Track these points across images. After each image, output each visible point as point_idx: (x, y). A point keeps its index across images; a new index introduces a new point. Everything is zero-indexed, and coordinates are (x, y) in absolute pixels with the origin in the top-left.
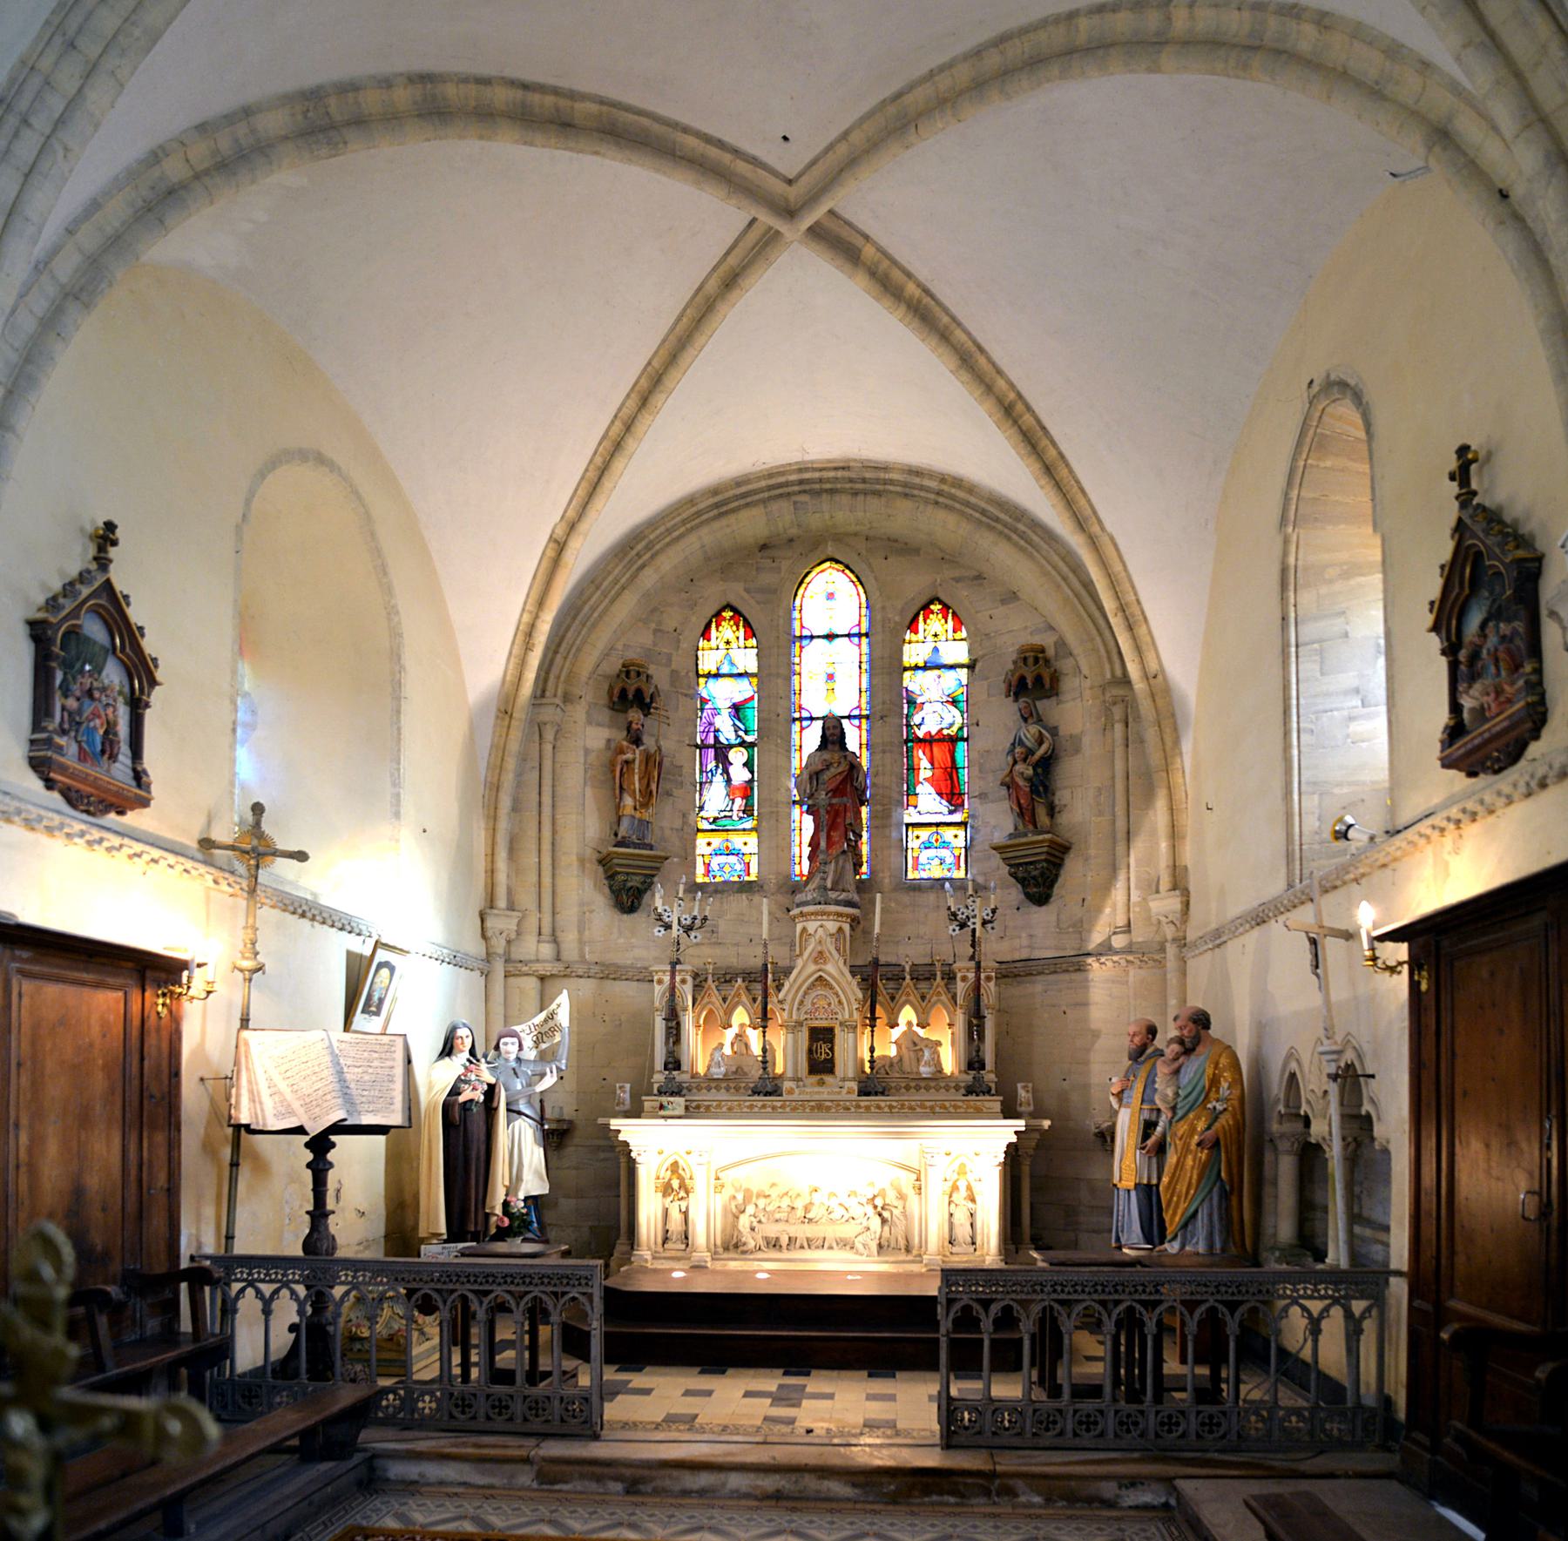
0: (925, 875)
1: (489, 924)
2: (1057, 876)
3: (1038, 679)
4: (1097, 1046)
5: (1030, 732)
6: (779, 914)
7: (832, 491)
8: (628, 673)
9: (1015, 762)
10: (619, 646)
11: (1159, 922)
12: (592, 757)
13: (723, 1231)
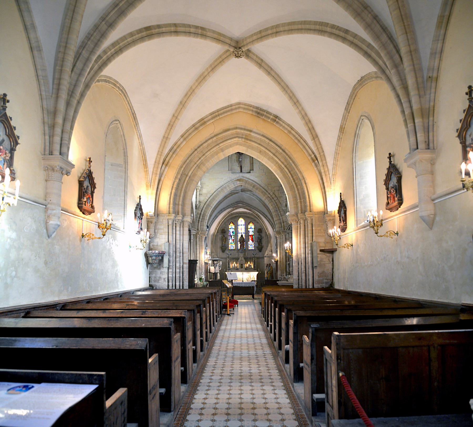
5: (259, 236)
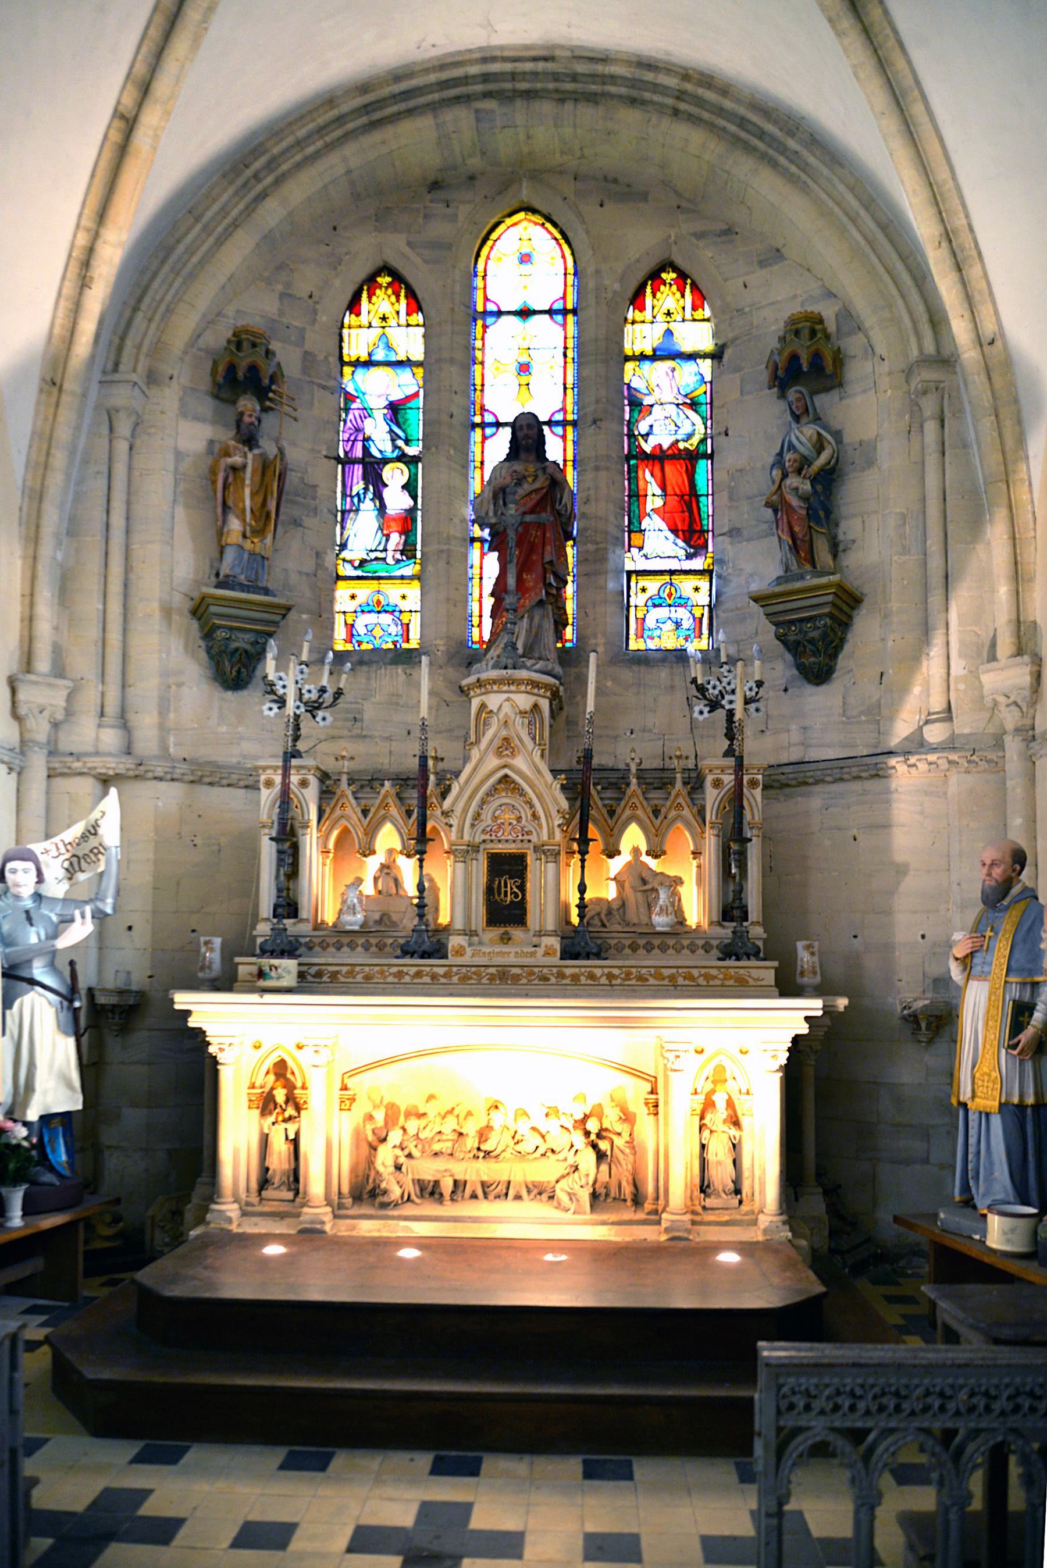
0: (652, 645)
1: (21, 696)
2: (842, 641)
3: (817, 359)
4: (902, 888)
6: (450, 696)
7: (529, 95)
8: (239, 345)
9: (785, 476)
10: (230, 310)
11: (996, 704)
12: (186, 465)
13: (353, 1170)
